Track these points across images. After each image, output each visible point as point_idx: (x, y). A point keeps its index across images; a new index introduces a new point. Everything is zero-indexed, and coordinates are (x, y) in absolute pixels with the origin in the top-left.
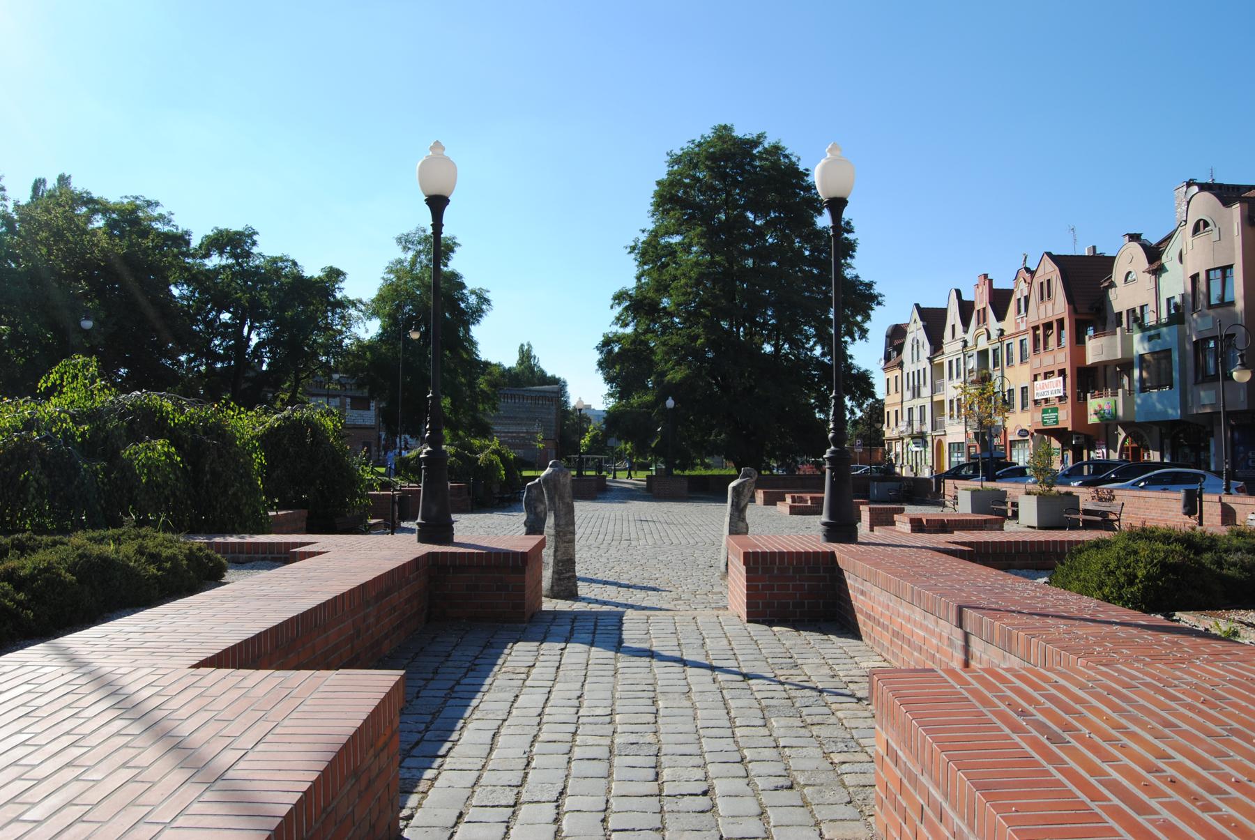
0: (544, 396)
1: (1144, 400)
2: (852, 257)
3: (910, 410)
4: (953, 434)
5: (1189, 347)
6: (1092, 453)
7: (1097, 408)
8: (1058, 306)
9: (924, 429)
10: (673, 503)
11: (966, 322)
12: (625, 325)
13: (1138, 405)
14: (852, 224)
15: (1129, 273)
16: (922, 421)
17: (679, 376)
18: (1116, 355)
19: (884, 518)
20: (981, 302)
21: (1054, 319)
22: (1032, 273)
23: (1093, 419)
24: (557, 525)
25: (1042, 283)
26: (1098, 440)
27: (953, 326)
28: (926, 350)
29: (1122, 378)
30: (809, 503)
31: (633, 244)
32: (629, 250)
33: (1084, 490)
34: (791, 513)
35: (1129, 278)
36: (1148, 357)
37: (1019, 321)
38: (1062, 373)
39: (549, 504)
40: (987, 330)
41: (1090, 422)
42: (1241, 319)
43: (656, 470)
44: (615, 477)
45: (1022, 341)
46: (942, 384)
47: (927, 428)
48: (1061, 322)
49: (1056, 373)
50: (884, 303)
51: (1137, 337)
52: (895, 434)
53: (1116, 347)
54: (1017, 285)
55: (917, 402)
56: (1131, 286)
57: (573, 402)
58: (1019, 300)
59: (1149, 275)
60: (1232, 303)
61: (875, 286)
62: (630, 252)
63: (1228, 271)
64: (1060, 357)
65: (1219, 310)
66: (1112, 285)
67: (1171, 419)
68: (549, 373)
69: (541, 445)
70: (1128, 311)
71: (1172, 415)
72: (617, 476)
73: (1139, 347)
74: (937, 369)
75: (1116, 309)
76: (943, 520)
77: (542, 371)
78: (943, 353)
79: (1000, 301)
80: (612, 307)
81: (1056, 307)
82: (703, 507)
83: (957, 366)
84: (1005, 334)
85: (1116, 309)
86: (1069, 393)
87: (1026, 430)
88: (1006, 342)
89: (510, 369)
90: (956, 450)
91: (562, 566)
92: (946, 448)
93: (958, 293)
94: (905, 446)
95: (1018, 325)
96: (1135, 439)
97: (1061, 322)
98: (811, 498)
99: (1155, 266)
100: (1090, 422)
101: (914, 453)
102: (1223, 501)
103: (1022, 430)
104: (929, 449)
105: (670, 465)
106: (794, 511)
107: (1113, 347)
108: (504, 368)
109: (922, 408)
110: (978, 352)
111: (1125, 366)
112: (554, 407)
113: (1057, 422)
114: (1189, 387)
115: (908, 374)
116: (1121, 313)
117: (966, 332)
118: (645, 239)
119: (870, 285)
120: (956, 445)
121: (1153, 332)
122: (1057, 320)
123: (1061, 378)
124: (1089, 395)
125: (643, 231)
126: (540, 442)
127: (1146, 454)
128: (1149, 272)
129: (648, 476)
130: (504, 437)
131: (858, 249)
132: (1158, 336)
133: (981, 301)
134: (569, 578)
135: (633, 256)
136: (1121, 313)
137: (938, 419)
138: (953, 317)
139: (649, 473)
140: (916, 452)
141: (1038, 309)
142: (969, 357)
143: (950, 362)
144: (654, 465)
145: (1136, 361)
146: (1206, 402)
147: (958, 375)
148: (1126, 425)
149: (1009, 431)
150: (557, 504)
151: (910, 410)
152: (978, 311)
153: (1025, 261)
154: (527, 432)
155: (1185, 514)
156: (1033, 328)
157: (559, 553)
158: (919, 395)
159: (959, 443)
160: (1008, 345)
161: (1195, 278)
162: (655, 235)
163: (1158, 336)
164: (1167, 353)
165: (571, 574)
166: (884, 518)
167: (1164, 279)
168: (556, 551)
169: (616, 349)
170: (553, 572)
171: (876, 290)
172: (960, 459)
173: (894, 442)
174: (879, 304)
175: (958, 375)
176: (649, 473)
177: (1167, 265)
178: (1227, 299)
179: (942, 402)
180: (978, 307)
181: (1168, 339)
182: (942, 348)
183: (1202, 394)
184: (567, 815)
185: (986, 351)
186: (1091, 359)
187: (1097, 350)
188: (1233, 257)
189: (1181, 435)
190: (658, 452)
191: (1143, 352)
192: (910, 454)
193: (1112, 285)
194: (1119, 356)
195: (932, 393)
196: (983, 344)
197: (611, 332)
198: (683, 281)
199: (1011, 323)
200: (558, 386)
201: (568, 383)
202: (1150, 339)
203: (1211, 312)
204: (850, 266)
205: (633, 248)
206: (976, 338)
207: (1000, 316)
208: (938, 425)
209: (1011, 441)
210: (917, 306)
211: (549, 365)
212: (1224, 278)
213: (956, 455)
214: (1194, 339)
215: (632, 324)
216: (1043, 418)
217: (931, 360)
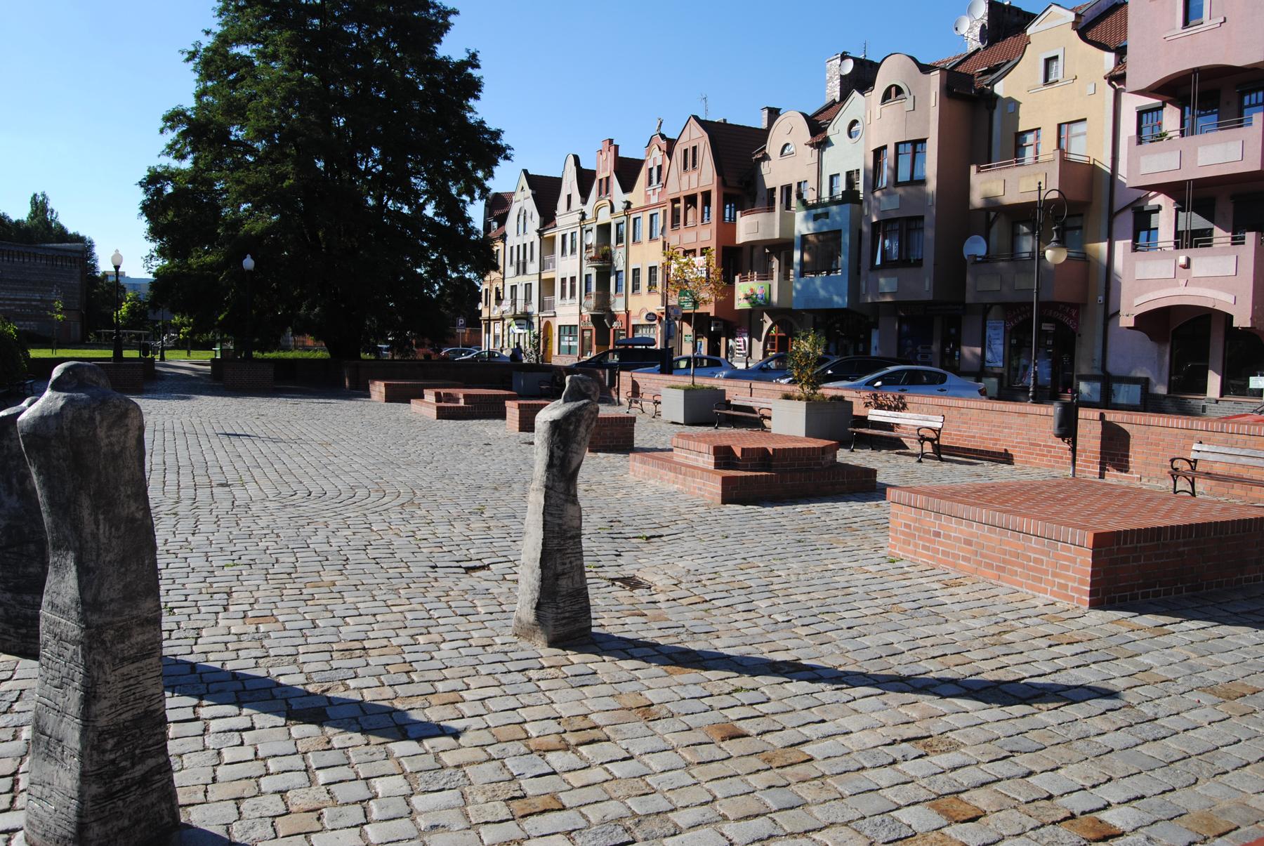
0: (65, 255)
1: (805, 286)
2: (477, 98)
3: (514, 288)
4: (564, 316)
5: (865, 229)
6: (731, 341)
7: (749, 293)
8: (705, 177)
9: (530, 309)
11: (585, 194)
12: (182, 157)
13: (797, 291)
14: (479, 57)
15: (787, 145)
16: (528, 299)
17: (259, 226)
18: (773, 235)
19: (608, 433)
21: (699, 191)
22: (671, 143)
23: (741, 304)
24: (88, 604)
25: (686, 151)
26: (739, 327)
27: (569, 197)
28: (535, 221)
29: (770, 262)
30: (462, 403)
31: (192, 49)
32: (186, 56)
33: (730, 382)
34: (439, 417)
35: (786, 151)
36: (811, 238)
37: (651, 193)
39: (56, 527)
40: (610, 201)
41: (737, 307)
42: (932, 200)
43: (222, 350)
44: (162, 358)
45: (652, 216)
46: (553, 261)
47: (534, 308)
49: (698, 252)
51: (800, 215)
52: (496, 313)
53: (773, 225)
54: (649, 154)
55: (522, 280)
56: (787, 161)
57: (104, 265)
58: (651, 170)
59: (810, 149)
60: (923, 182)
61: (503, 136)
62: (188, 60)
63: (919, 146)
64: (701, 233)
65: (909, 189)
66: (766, 157)
67: (835, 307)
68: (71, 230)
69: (59, 316)
70: (782, 187)
72: (166, 356)
73: (802, 226)
74: (548, 245)
75: (769, 185)
76: (765, 450)
77: (62, 228)
78: (555, 226)
79: (627, 171)
80: (162, 131)
81: (703, 177)
82: (303, 404)
83: (572, 241)
84: (632, 207)
85: (769, 185)
87: (654, 314)
88: (633, 217)
89: (18, 222)
90: (567, 333)
91: (117, 746)
92: (556, 331)
93: (576, 158)
94: (506, 327)
95: (648, 197)
96: (781, 328)
97: (707, 196)
98: (465, 396)
99: (819, 138)
100: (737, 307)
101: (516, 336)
102: (1107, 419)
103: (649, 314)
105: (245, 345)
106: (443, 414)
107: (770, 226)
108: (10, 221)
109: (528, 286)
110: (598, 226)
111: (782, 248)
114: (863, 273)
115: (512, 248)
116: (774, 189)
117: (584, 202)
118: (209, 45)
119: (497, 134)
120: (567, 328)
121: (820, 211)
122: (685, 197)
124: (737, 278)
125: (208, 33)
126: (59, 313)
128: (811, 145)
130: (9, 305)
131: (484, 89)
132: (826, 215)
133: (604, 168)
134: (145, 780)
135: (191, 65)
136: (774, 189)
137: (547, 299)
138: (570, 186)
140: (519, 334)
141: (680, 179)
142: (587, 231)
143: (564, 237)
144: (218, 345)
145: (797, 242)
146: (887, 290)
147: (573, 251)
148: (774, 312)
149: (632, 314)
150: (88, 528)
151: (514, 288)
152: (601, 180)
153: (660, 126)
154: (41, 301)
155: (1058, 436)
156: (672, 200)
157: (98, 707)
158: (524, 272)
159: (570, 326)
160: (635, 220)
161: (878, 153)
162: (224, 40)
163: (826, 215)
164: (837, 234)
165: (151, 762)
166: (608, 433)
167: (828, 153)
168: (89, 698)
169: (169, 189)
170: (83, 776)
171: (504, 140)
172: (571, 344)
173: (492, 323)
174: (507, 158)
175: (573, 251)
177: (832, 139)
178: (917, 175)
179: (553, 280)
180: (601, 175)
181: (838, 218)
183: (882, 281)
185: (609, 225)
186: (742, 236)
187: (748, 228)
188: (927, 130)
189: (838, 325)
190: (224, 327)
191: (805, 232)
192: (511, 336)
193: (766, 157)
194: (777, 236)
196: (604, 217)
197: (160, 166)
198: (266, 100)
199: (638, 196)
200: (81, 250)
201: (97, 242)
202: (816, 218)
203: (900, 191)
204: (471, 110)
205: (193, 55)
206: (597, 210)
207: (627, 187)
208: (546, 306)
210: (525, 172)
211: (71, 219)
212: (915, 152)
213: (567, 338)
214: (874, 219)
215: (191, 156)
217: (540, 233)
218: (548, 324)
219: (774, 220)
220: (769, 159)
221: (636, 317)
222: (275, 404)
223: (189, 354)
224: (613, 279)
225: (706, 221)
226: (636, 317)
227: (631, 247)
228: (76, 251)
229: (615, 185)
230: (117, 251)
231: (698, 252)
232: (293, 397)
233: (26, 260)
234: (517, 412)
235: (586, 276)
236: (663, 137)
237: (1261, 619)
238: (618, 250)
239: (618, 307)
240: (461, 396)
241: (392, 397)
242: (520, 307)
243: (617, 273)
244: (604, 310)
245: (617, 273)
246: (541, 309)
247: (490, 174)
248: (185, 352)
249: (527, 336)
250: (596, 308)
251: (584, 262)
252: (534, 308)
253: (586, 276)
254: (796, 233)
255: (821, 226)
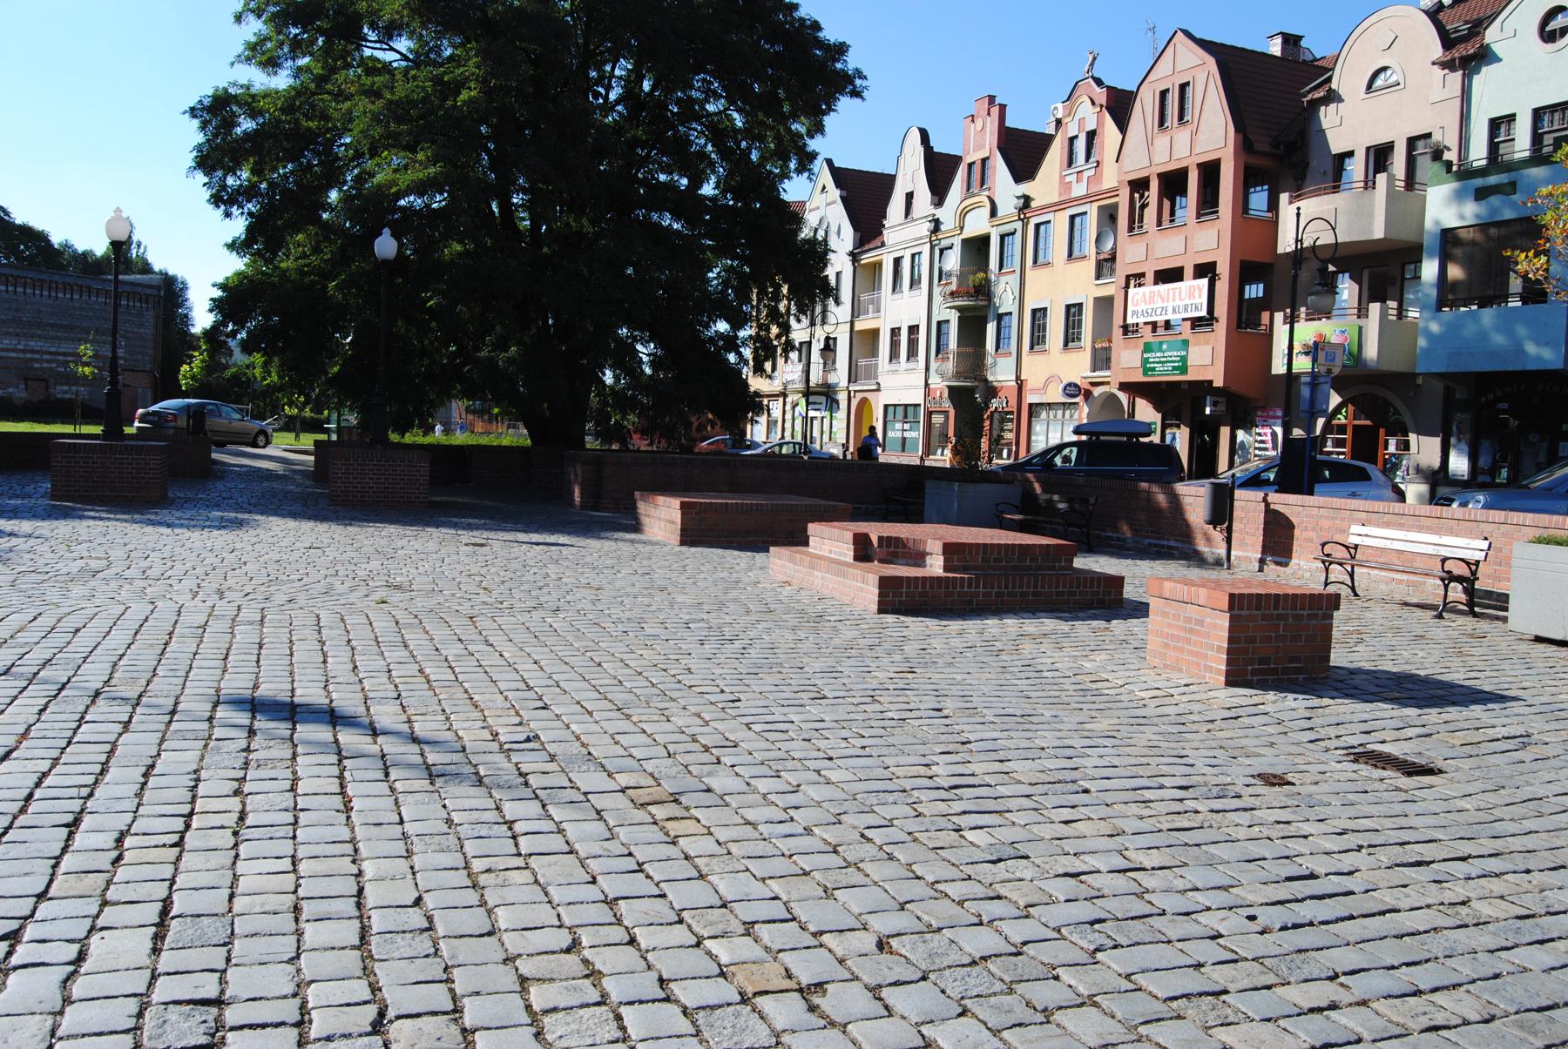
9: (832, 379)
10: (392, 530)
11: (939, 190)
15: (1384, 69)
18: (1371, 231)
20: (979, 147)
21: (1192, 163)
25: (1164, 94)
27: (910, 196)
30: (935, 566)
35: (1379, 83)
37: (1073, 178)
38: (1206, 270)
40: (989, 197)
43: (339, 430)
45: (1072, 218)
47: (840, 376)
48: (1210, 172)
49: (1189, 272)
50: (865, 94)
53: (1371, 215)
56: (1382, 101)
58: (1072, 140)
67: (1531, 367)
70: (1368, 149)
71: (1539, 358)
78: (883, 245)
80: (238, 18)
81: (1202, 137)
83: (913, 267)
84: (1033, 204)
85: (1337, 146)
86: (1221, 310)
87: (1076, 385)
92: (879, 413)
93: (924, 135)
94: (788, 407)
97: (1210, 172)
98: (950, 550)
103: (1069, 385)
104: (841, 415)
108: (75, 251)
110: (964, 241)
112: (152, 313)
113: (1184, 369)
119: (841, 49)
120: (900, 411)
122: (1160, 175)
123: (1204, 282)
126: (87, 364)
127: (1392, 442)
129: (317, 443)
130: (47, 361)
138: (912, 176)
139: (323, 437)
141: (1150, 144)
143: (897, 262)
147: (914, 283)
153: (1092, 64)
156: (1130, 183)
159: (906, 406)
160: (1037, 226)
172: (907, 435)
174: (856, 94)
175: (914, 283)
176: (323, 437)
179: (875, 333)
182: (881, 233)
184: (162, 978)
185: (984, 241)
191: (1451, 221)
193: (1332, 97)
194: (1378, 233)
195: (853, 316)
196: (978, 224)
199: (1046, 184)
201: (191, 283)
202: (1481, 194)
208: (862, 372)
209: (1031, 405)
213: (898, 426)
216: (1145, 361)
217: (854, 256)
218: (864, 401)
219: (1372, 204)
220: (1340, 100)
221: (1035, 391)
222: (432, 546)
223: (297, 437)
224: (991, 328)
225: (1166, 224)
226: (1035, 391)
227: (1030, 274)
228: (150, 287)
229: (1000, 171)
230: (118, 210)
231: (1189, 272)
232: (470, 527)
233: (76, 297)
234: (1224, 621)
235: (939, 324)
236: (1099, 82)
237: (4, 354)
238: (1003, 279)
239: (1001, 372)
240: (934, 548)
241: (695, 533)
242: (816, 377)
243: (1000, 317)
244: (975, 379)
245: (1000, 317)
246: (853, 377)
247: (817, 129)
248: (293, 435)
249: (827, 422)
250: (958, 375)
251: (937, 299)
252: (840, 376)
253: (939, 324)
254: (1429, 224)
255: (1494, 211)
